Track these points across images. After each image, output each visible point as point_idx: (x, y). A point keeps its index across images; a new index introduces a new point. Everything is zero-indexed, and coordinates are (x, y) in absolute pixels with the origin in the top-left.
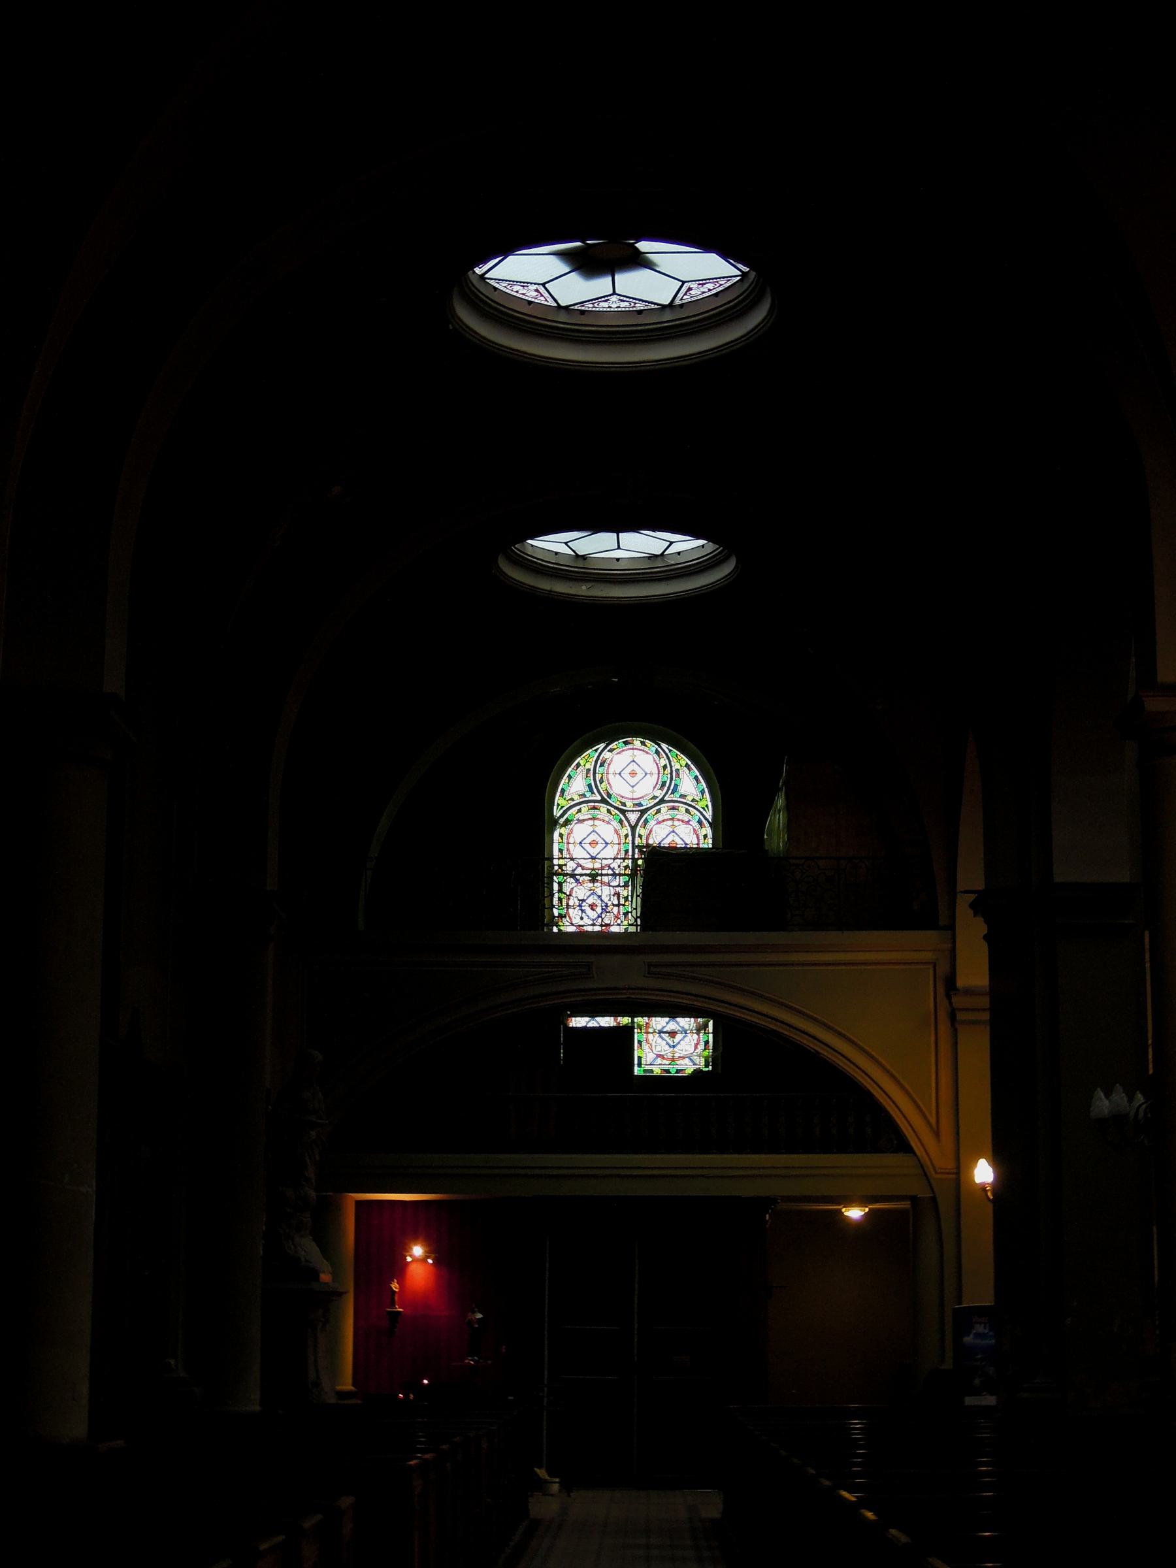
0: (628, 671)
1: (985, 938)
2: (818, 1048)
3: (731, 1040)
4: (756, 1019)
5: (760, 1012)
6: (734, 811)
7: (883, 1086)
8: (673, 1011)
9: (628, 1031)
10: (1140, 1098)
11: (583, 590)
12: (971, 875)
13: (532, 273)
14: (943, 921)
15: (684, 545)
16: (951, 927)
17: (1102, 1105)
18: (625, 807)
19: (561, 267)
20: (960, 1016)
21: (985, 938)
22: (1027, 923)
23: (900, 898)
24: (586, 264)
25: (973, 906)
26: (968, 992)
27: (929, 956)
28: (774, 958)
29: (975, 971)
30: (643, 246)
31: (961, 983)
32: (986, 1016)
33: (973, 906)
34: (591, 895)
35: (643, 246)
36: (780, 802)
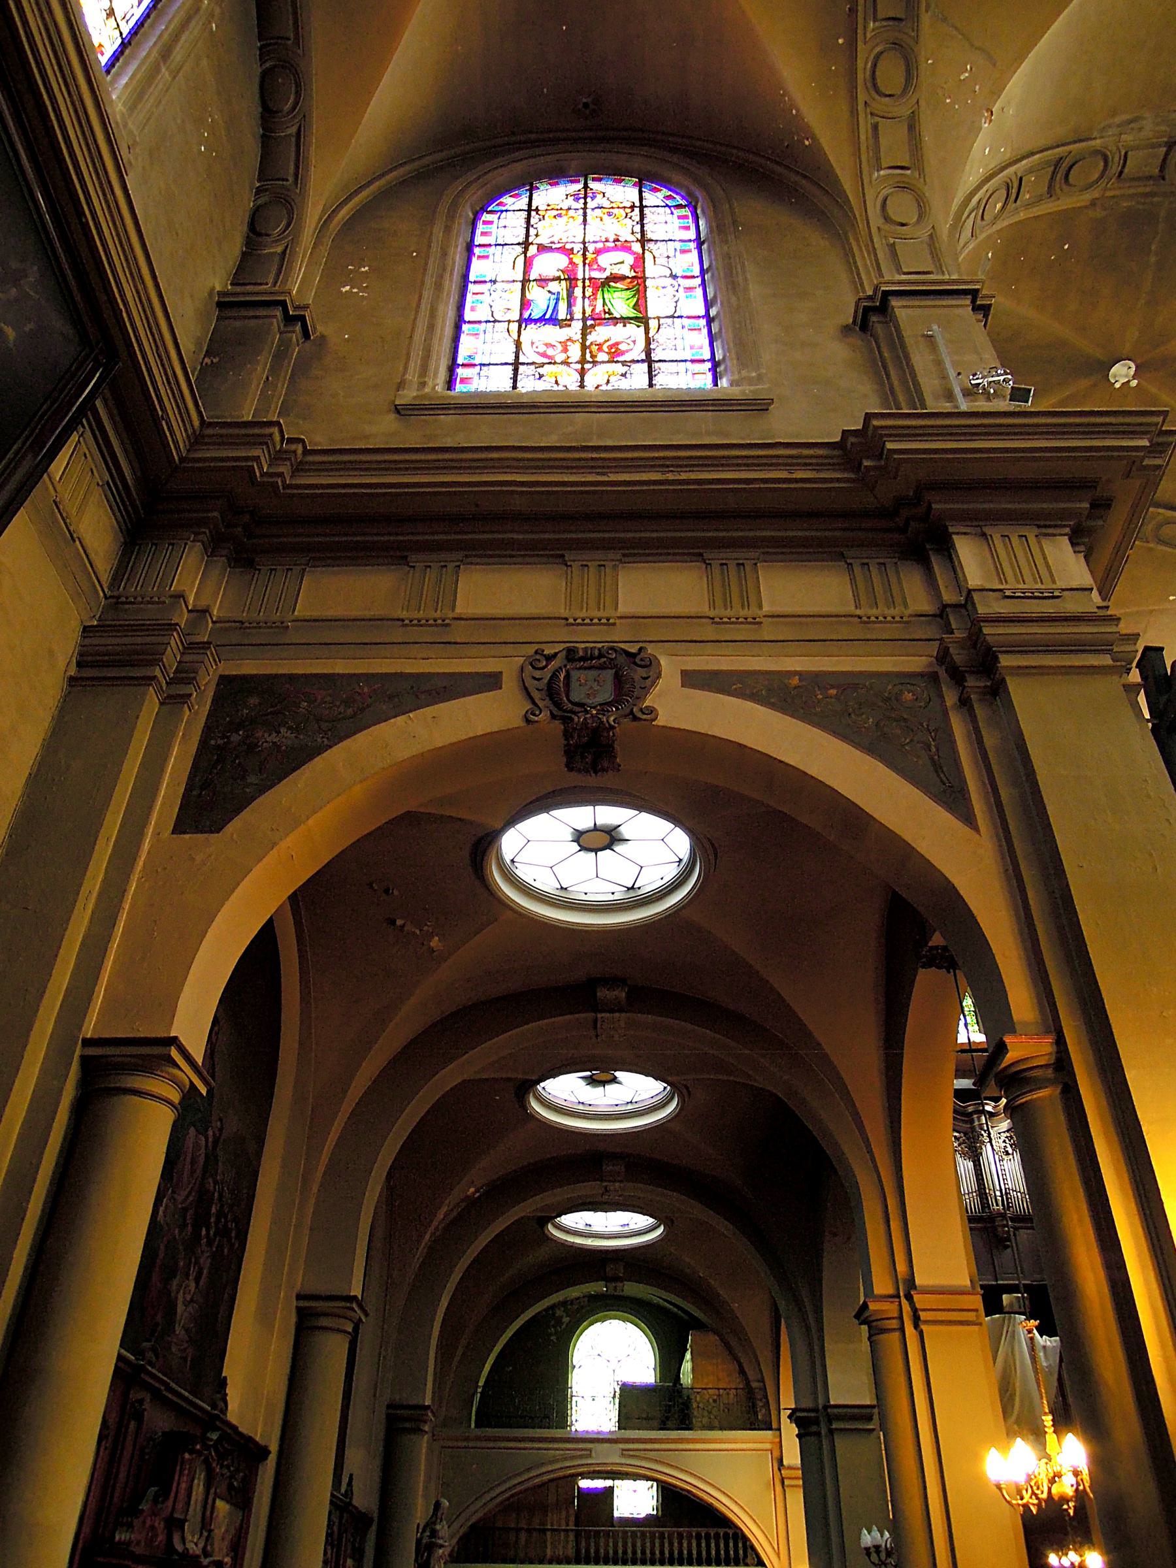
0: (610, 1284)
1: (797, 1436)
2: (711, 1500)
3: (670, 1496)
4: (678, 1483)
5: (683, 1479)
6: (669, 1361)
7: (939, 1313)
8: (636, 1477)
9: (611, 1489)
10: (887, 1534)
11: (589, 1242)
12: (788, 1401)
13: (567, 1088)
14: (774, 1426)
15: (640, 1221)
16: (779, 1429)
17: (868, 1539)
18: (610, 1359)
19: (582, 1083)
20: (787, 1482)
21: (797, 1436)
22: (816, 1423)
23: (752, 1413)
24: (592, 1081)
25: (790, 1417)
26: (790, 1468)
27: (768, 1446)
28: (698, 1446)
29: (793, 1455)
30: (617, 1074)
31: (785, 1463)
32: (801, 1482)
33: (790, 1417)
34: (592, 1409)
35: (617, 1074)
36: (688, 1356)
